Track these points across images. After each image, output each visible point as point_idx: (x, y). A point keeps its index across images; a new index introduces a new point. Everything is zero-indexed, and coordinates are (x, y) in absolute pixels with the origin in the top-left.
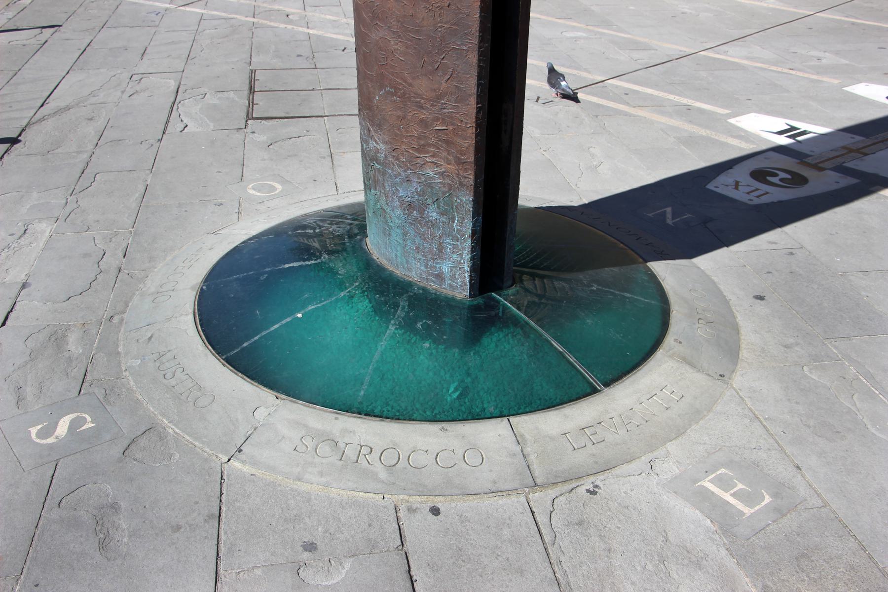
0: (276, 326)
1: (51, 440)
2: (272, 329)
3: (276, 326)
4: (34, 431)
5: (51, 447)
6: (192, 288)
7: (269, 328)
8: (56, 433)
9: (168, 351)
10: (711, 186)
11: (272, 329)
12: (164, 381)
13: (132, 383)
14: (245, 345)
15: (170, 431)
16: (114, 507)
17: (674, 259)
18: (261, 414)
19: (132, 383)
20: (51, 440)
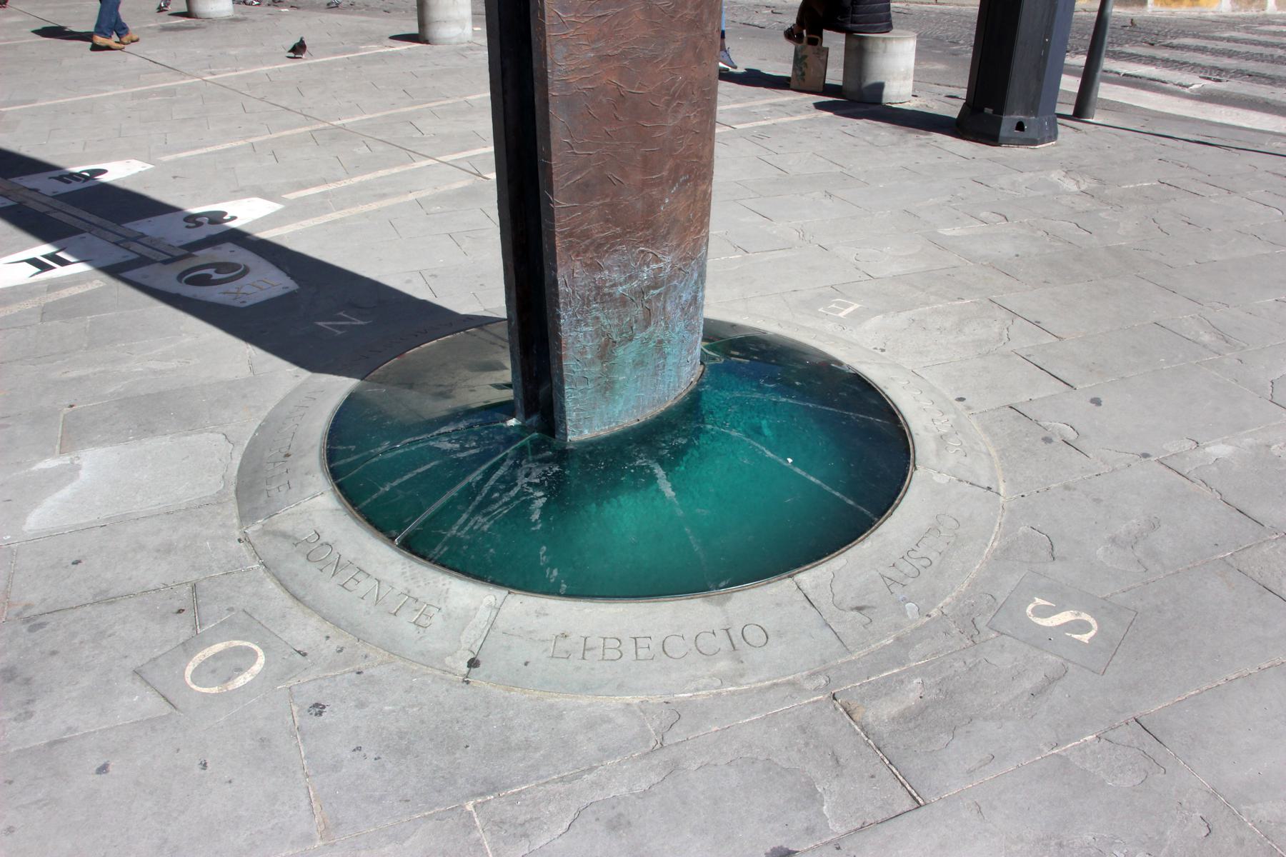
0: (813, 479)
1: (1085, 617)
2: (818, 482)
3: (813, 479)
4: (1085, 638)
5: (1093, 613)
6: (720, 604)
7: (820, 487)
8: (1073, 618)
9: (883, 577)
10: (292, 285)
11: (818, 482)
12: (935, 563)
13: (948, 600)
14: (851, 502)
15: (996, 544)
16: (1113, 540)
17: (339, 374)
18: (942, 479)
19: (948, 600)
20: (1085, 617)
